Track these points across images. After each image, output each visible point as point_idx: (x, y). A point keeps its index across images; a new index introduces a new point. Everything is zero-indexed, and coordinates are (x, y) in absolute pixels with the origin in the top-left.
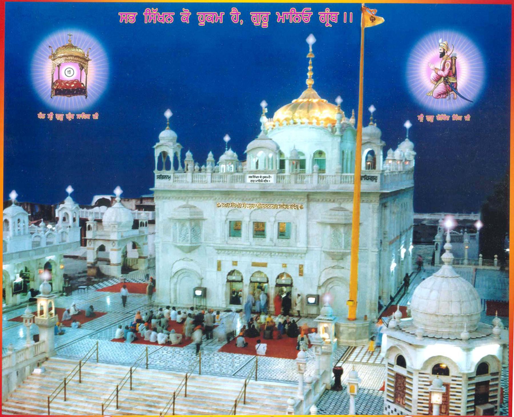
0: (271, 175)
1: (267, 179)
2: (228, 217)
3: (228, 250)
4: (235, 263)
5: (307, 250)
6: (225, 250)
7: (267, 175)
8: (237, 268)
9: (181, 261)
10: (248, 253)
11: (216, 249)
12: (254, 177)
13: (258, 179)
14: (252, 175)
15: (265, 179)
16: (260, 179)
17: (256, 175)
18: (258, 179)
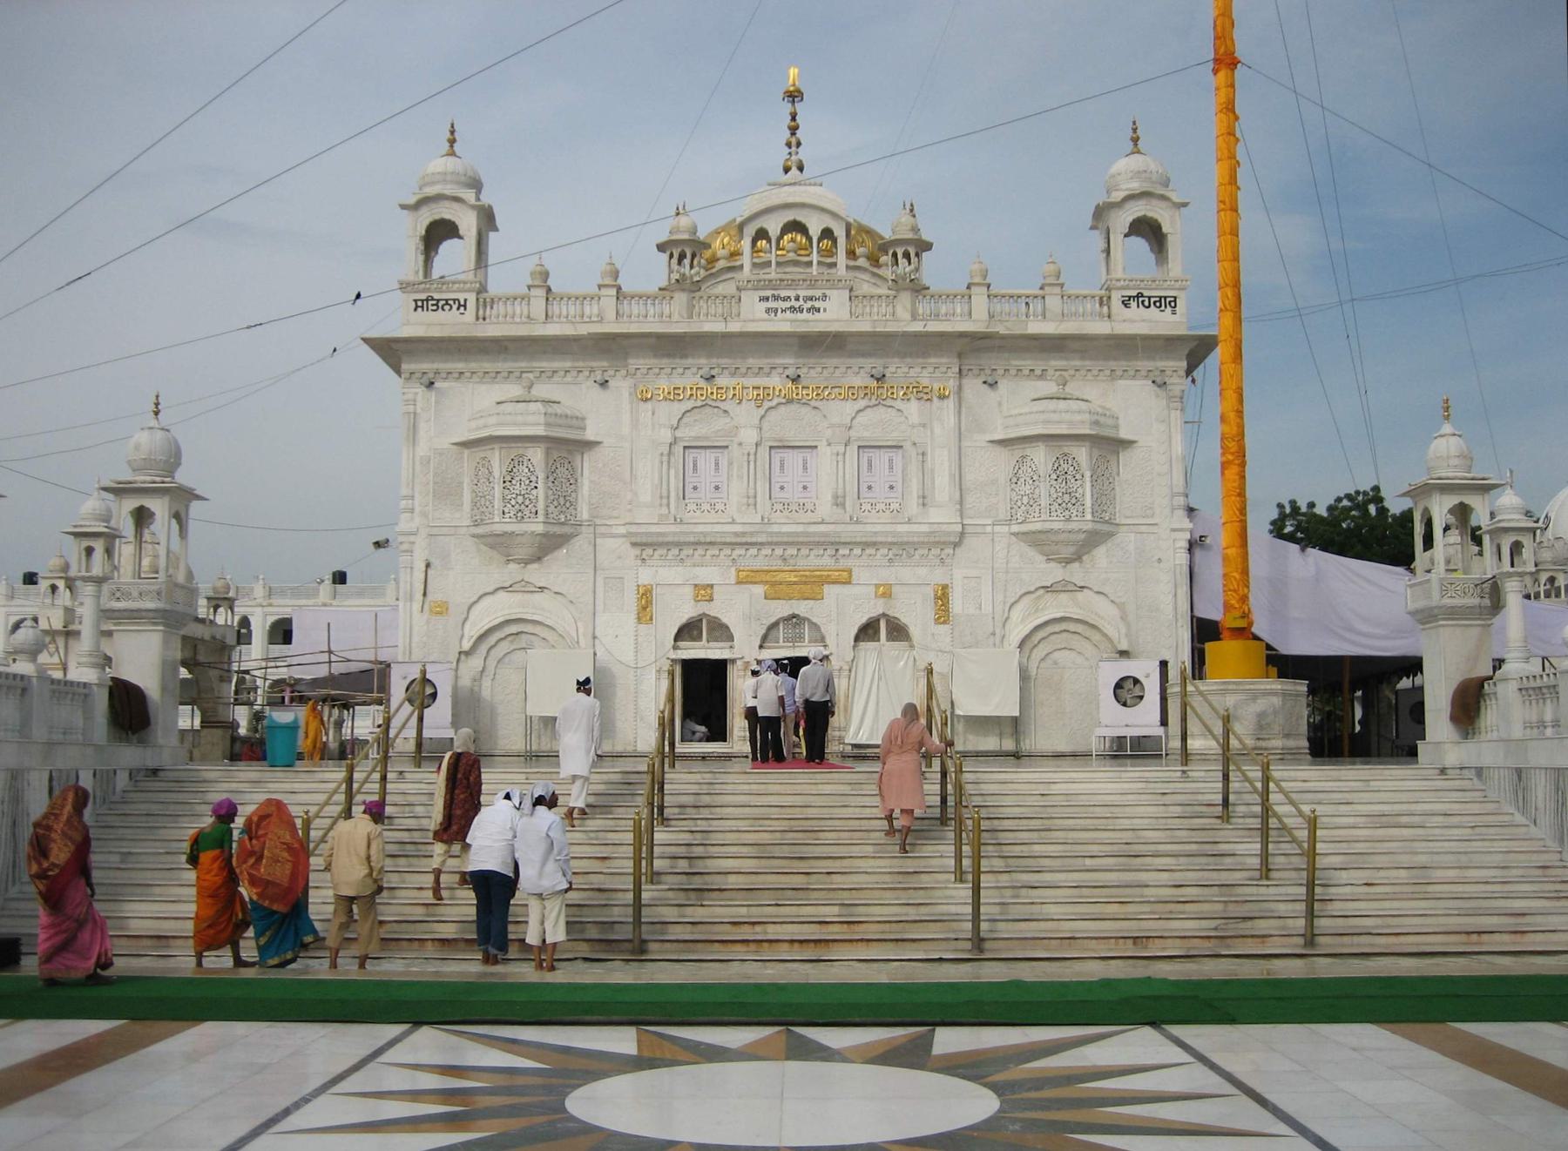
0: (828, 292)
1: (817, 304)
2: (678, 434)
3: (680, 545)
4: (704, 592)
5: (962, 534)
6: (668, 545)
7: (818, 293)
8: (714, 610)
9: (501, 594)
10: (753, 551)
11: (634, 544)
12: (776, 298)
13: (787, 304)
14: (769, 293)
15: (809, 304)
16: (797, 305)
17: (783, 293)
18: (787, 304)
